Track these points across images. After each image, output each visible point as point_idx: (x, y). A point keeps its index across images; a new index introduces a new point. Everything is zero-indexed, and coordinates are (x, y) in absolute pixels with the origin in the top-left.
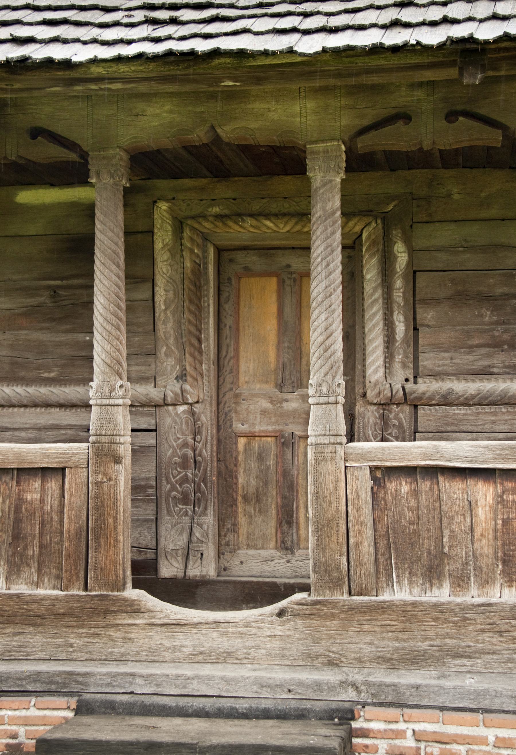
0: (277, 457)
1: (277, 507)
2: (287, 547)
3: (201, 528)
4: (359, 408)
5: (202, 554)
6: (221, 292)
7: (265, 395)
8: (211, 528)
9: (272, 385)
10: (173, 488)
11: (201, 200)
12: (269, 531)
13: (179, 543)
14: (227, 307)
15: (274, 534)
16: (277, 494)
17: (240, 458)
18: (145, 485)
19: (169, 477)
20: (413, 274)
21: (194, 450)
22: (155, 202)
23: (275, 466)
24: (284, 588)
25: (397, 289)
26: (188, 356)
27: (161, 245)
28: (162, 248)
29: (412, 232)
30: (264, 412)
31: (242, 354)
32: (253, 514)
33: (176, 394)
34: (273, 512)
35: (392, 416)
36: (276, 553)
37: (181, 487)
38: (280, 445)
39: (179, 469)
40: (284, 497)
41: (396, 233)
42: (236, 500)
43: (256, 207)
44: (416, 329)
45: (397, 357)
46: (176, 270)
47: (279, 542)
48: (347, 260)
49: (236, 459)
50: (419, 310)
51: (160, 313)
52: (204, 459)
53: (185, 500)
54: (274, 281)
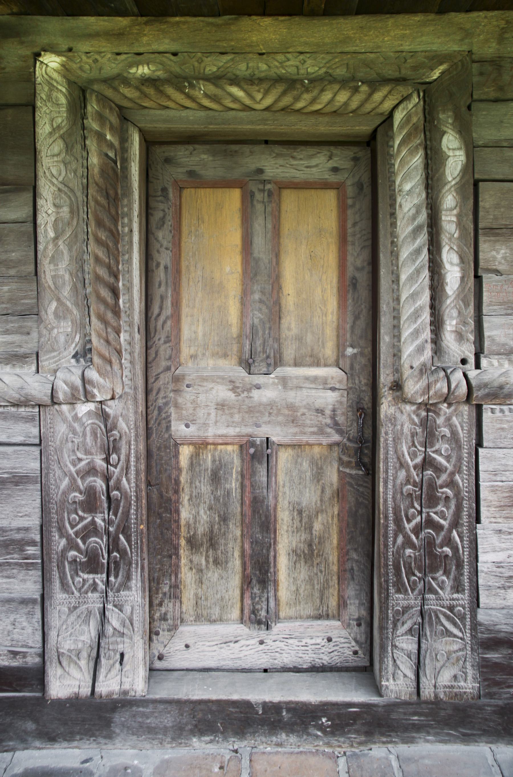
0: (243, 476)
1: (243, 555)
2: (259, 619)
3: (121, 610)
4: (386, 408)
5: (122, 655)
6: (150, 211)
7: (223, 378)
8: (138, 611)
9: (234, 360)
10: (72, 545)
11: (118, 54)
12: (230, 593)
13: (82, 638)
14: (160, 234)
15: (239, 598)
16: (242, 535)
17: (184, 478)
18: (23, 540)
19: (64, 526)
20: (473, 187)
21: (107, 479)
22: (39, 55)
23: (239, 490)
24: (263, 709)
25: (447, 210)
26: (94, 319)
27: (48, 129)
28: (50, 133)
29: (471, 115)
30: (221, 406)
31: (185, 310)
32: (204, 567)
33: (73, 388)
34: (236, 563)
35: (440, 421)
36: (242, 630)
37: (84, 543)
38: (248, 458)
39: (80, 513)
40: (254, 542)
41: (446, 118)
42: (176, 548)
43: (212, 66)
44: (478, 278)
45: (448, 322)
46: (75, 172)
47: (246, 611)
48: (352, 163)
49: (177, 482)
50: (483, 246)
51: (47, 243)
52: (125, 495)
53: (92, 564)
54: (236, 194)
